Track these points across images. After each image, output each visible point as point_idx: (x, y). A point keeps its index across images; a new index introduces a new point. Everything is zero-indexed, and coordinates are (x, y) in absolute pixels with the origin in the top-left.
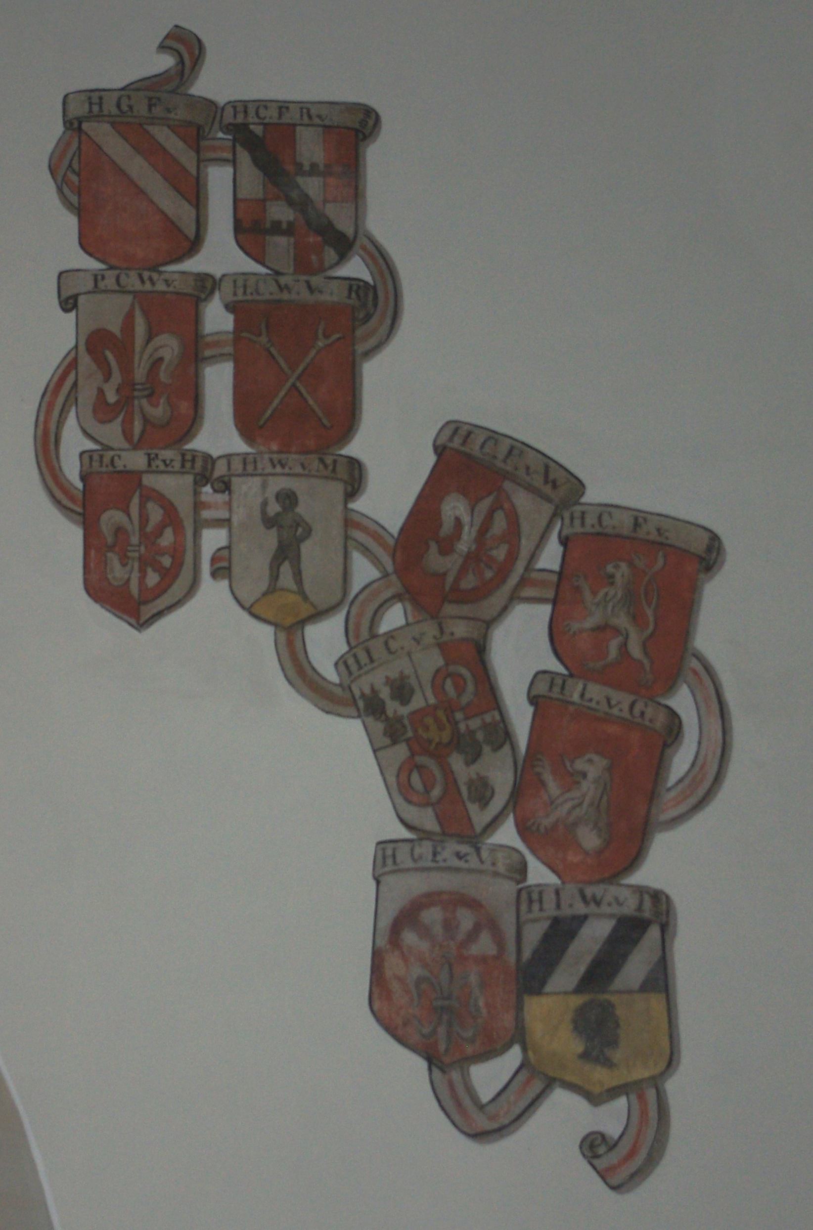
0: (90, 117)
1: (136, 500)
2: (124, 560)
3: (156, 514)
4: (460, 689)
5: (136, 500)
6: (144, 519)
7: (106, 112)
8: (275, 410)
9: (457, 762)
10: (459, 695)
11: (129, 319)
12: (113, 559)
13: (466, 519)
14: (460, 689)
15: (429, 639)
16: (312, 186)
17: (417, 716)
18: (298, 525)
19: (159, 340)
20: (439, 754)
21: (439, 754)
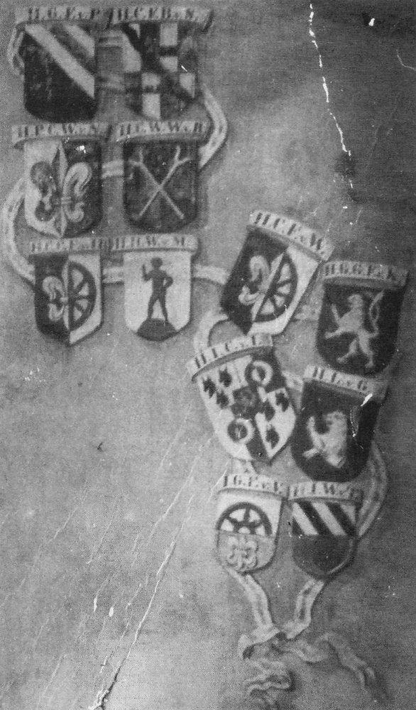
0: (30, 22)
1: (279, 258)
2: (59, 305)
3: (78, 277)
4: (262, 374)
5: (279, 258)
6: (71, 281)
7: (40, 18)
8: (172, 211)
9: (260, 418)
10: (262, 379)
11: (57, 157)
12: (52, 307)
13: (59, 288)
14: (262, 374)
15: (28, 412)
16: (170, 63)
17: (236, 394)
18: (163, 279)
19: (75, 168)
20: (250, 414)
21: (250, 414)
